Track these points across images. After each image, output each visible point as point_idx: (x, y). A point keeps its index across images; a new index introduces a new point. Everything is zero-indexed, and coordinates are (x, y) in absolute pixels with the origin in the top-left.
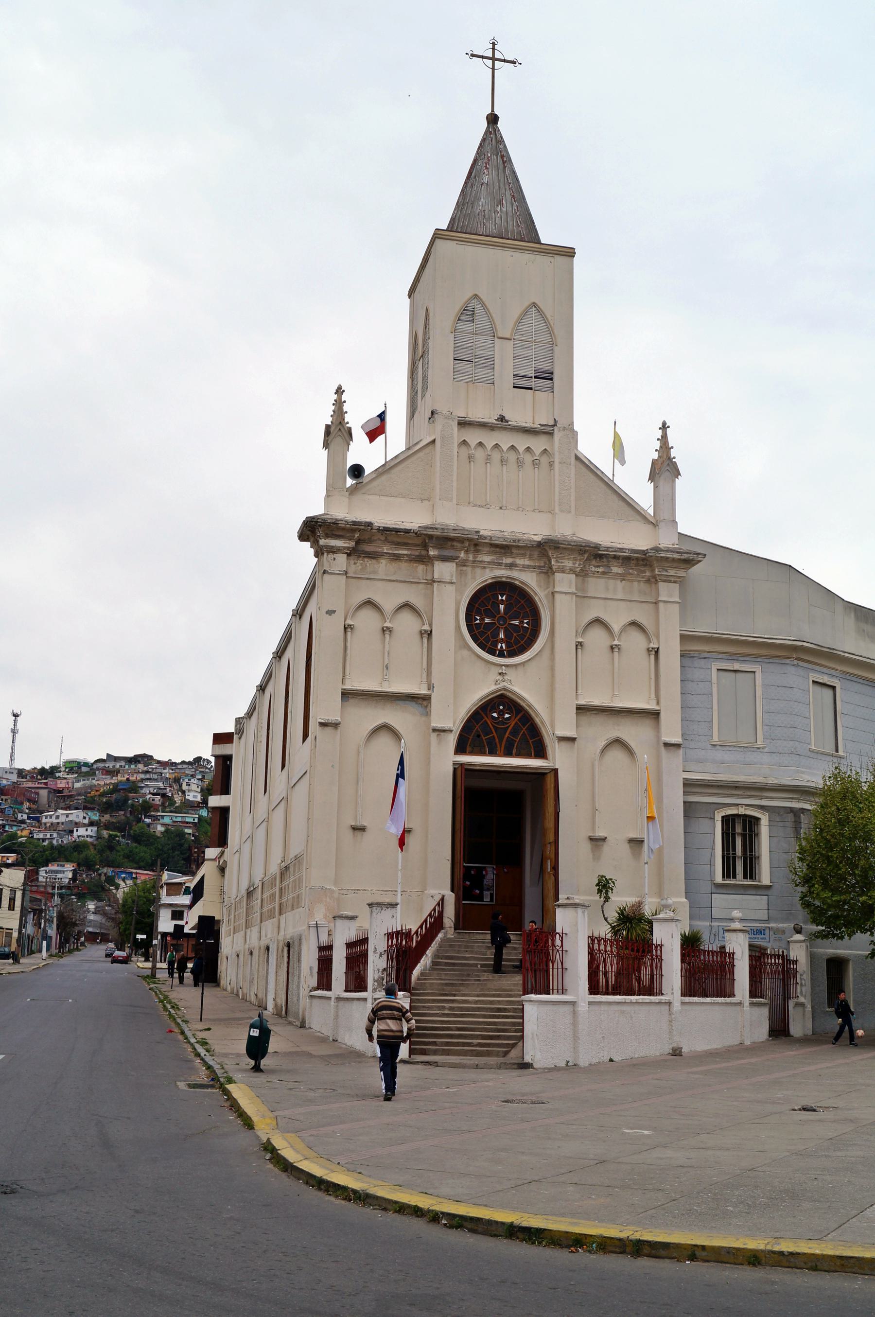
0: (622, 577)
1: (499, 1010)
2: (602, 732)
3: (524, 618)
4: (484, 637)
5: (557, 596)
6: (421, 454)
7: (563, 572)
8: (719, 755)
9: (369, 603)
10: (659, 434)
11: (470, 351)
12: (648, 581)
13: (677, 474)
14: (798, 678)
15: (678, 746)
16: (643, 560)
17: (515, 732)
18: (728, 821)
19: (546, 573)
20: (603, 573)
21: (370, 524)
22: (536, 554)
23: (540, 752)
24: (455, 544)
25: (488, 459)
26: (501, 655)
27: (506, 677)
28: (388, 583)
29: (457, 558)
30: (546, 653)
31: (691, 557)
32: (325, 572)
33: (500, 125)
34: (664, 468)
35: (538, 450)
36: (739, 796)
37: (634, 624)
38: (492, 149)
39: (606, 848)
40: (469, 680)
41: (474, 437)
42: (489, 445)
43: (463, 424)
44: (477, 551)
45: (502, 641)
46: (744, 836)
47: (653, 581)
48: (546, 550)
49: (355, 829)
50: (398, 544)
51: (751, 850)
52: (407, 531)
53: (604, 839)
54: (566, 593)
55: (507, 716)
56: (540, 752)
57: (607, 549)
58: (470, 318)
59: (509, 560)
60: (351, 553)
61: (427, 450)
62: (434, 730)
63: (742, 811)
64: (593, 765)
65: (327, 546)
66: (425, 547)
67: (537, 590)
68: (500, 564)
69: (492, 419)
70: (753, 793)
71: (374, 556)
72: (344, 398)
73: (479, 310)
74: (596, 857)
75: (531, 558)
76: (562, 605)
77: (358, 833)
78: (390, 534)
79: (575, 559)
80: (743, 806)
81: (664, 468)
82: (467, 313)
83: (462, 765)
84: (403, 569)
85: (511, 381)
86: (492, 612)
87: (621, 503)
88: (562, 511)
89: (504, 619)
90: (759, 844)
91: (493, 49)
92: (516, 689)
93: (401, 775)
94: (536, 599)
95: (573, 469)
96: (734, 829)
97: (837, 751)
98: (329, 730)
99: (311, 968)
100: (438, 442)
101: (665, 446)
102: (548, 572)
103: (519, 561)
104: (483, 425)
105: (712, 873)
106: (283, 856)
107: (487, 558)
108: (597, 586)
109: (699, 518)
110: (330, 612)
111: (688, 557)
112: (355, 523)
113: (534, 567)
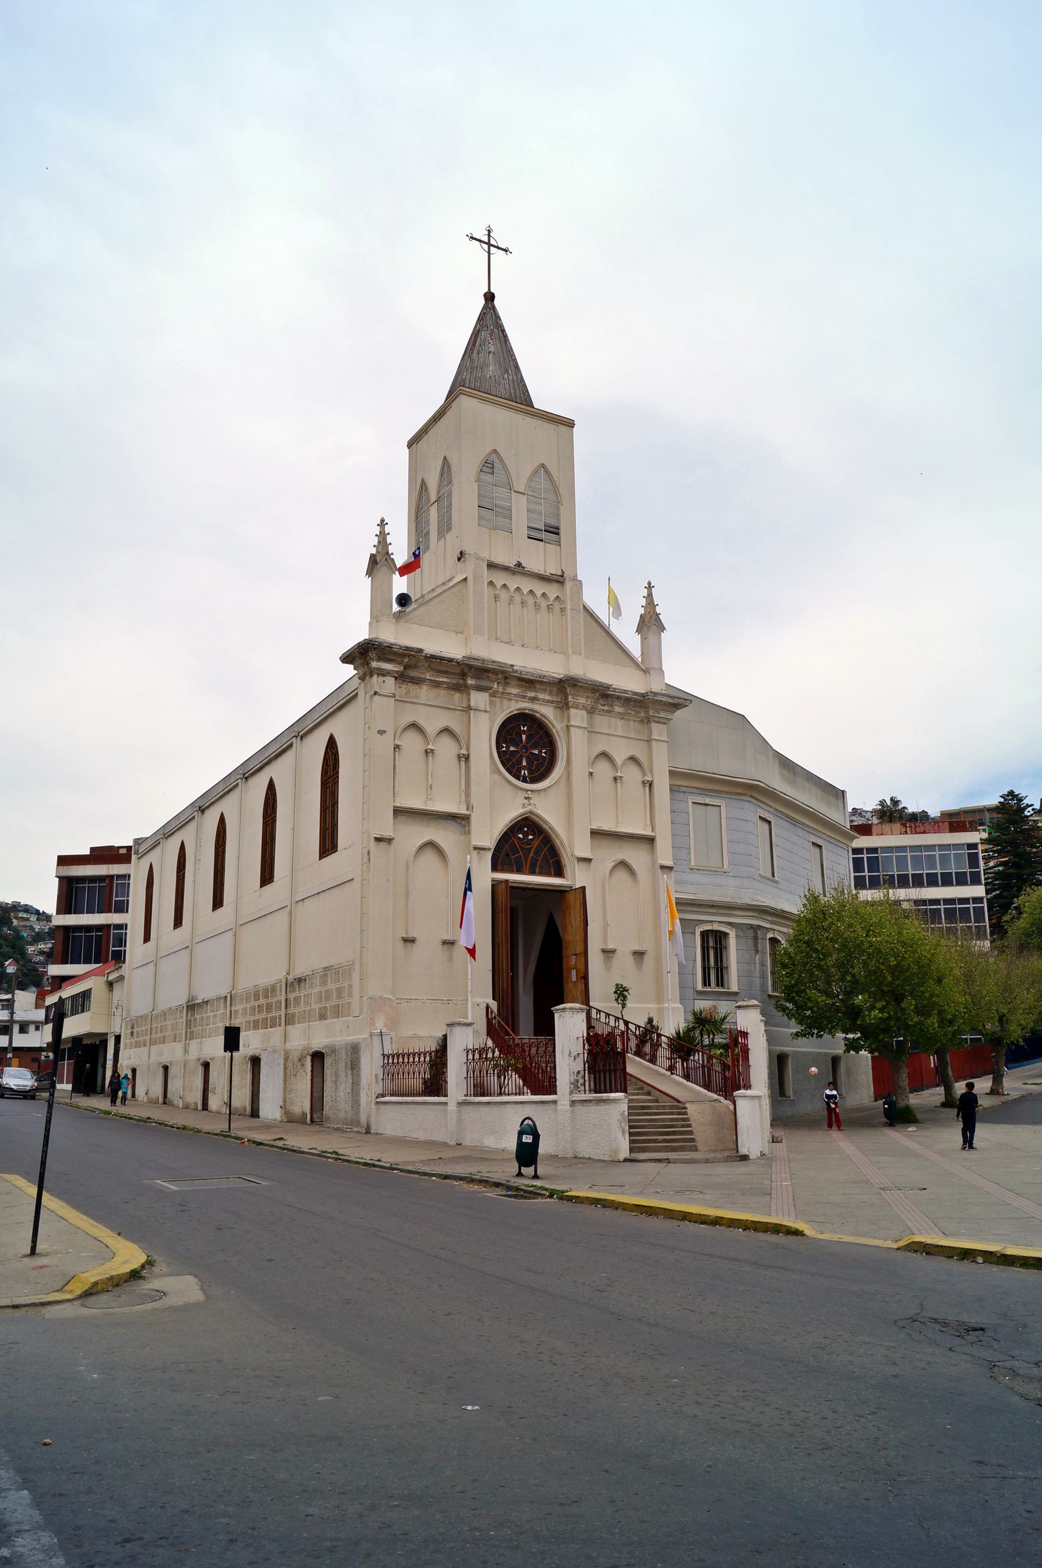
0: (622, 716)
1: (643, 1108)
2: (609, 855)
3: (544, 747)
4: (510, 762)
5: (572, 729)
6: (454, 590)
8: (696, 877)
9: (414, 726)
10: (645, 592)
12: (642, 721)
13: (663, 628)
14: (750, 811)
15: (670, 868)
16: (640, 701)
17: (537, 852)
18: (705, 935)
19: (561, 708)
20: (609, 712)
21: (420, 651)
22: (555, 690)
23: (559, 871)
24: (490, 675)
25: (511, 600)
26: (524, 780)
27: (532, 802)
28: (431, 708)
29: (490, 688)
30: (563, 781)
31: (681, 701)
32: (376, 693)
33: (496, 302)
34: (650, 623)
35: (552, 596)
36: (715, 914)
37: (632, 759)
38: (489, 321)
39: (616, 959)
41: (500, 579)
42: (512, 587)
43: (491, 566)
44: (507, 684)
45: (525, 768)
46: (715, 949)
47: (647, 721)
48: (564, 688)
49: (406, 940)
50: (440, 672)
51: (721, 961)
52: (450, 660)
53: (613, 951)
54: (580, 727)
55: (530, 837)
56: (559, 871)
58: (490, 470)
59: (531, 694)
60: (401, 677)
61: (459, 587)
62: (475, 848)
64: (603, 884)
65: (378, 669)
66: (463, 675)
67: (555, 723)
68: (524, 697)
69: (512, 564)
70: (725, 911)
71: (417, 681)
72: (387, 529)
73: (496, 461)
74: (608, 968)
75: (550, 694)
76: (576, 736)
77: (409, 945)
78: (436, 661)
79: (588, 697)
80: (716, 922)
81: (650, 623)
82: (489, 465)
83: (500, 882)
84: (441, 696)
85: (525, 532)
86: (516, 742)
88: (574, 653)
89: (527, 748)
90: (727, 957)
91: (489, 235)
92: (540, 812)
93: (468, 888)
94: (554, 731)
95: (582, 614)
97: (773, 876)
98: (383, 845)
99: (376, 1075)
100: (470, 581)
101: (650, 602)
102: (564, 706)
103: (541, 696)
104: (506, 569)
105: (694, 982)
106: (287, 968)
107: (514, 691)
108: (602, 722)
109: (682, 671)
110: (381, 732)
111: (677, 702)
112: (408, 649)
113: (552, 702)
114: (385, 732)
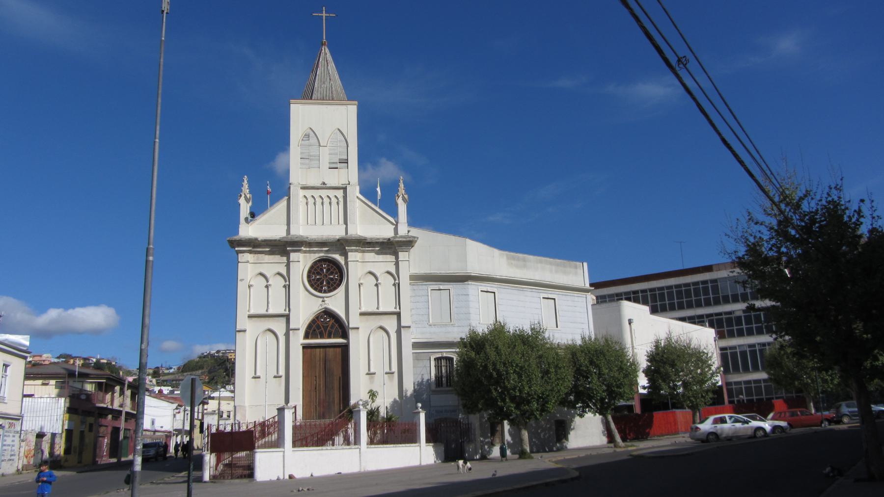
17: (332, 327)
26: (325, 292)
40: (306, 306)
41: (309, 193)
52: (275, 240)
57: (371, 239)
63: (445, 355)
69: (318, 184)
74: (372, 381)
76: (358, 265)
82: (307, 136)
85: (328, 166)
87: (727, 101)
89: (327, 275)
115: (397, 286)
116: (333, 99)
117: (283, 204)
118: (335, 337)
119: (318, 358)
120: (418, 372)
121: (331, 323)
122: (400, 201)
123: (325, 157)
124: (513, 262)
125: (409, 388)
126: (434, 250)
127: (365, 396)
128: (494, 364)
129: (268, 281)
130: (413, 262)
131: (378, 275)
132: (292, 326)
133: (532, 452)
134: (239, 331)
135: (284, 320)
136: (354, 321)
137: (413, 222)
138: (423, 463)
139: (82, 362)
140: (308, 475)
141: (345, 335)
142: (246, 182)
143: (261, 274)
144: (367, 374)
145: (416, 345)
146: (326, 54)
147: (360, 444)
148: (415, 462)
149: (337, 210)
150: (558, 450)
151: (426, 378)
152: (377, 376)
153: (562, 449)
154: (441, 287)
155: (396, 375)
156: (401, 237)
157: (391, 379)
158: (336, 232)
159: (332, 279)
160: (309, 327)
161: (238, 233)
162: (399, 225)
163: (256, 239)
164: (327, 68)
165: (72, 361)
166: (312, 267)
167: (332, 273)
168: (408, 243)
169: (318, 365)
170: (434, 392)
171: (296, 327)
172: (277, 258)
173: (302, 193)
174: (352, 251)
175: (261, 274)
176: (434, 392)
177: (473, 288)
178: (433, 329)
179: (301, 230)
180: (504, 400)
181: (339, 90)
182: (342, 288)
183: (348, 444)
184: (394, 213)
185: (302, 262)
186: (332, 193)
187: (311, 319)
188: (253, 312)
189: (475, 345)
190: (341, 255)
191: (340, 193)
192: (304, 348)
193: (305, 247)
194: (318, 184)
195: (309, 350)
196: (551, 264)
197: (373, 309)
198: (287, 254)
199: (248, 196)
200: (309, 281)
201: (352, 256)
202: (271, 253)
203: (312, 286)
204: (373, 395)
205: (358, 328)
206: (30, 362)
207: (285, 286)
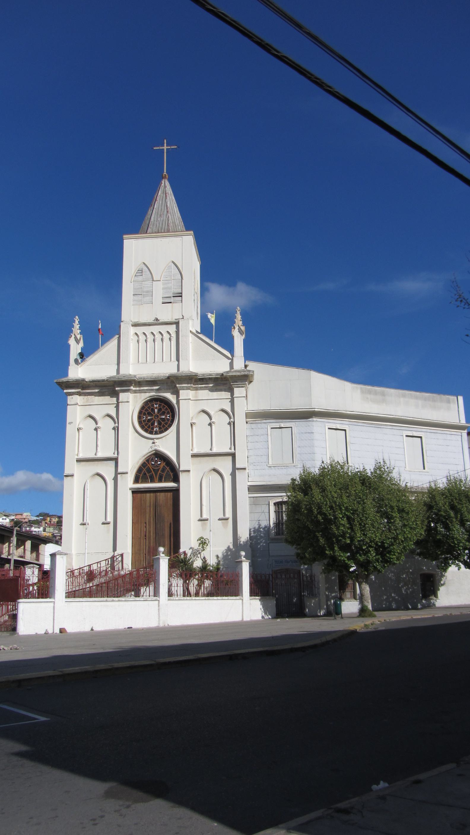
7: (184, 390)
11: (141, 290)
17: (163, 471)
26: (156, 433)
40: (135, 448)
41: (140, 330)
52: (103, 381)
57: (203, 375)
58: (141, 274)
76: (190, 404)
82: (140, 272)
85: (161, 301)
96: (282, 509)
114: (72, 423)
115: (232, 424)
116: (168, 231)
117: (114, 342)
118: (166, 481)
119: (148, 504)
120: (257, 516)
121: (162, 466)
122: (235, 333)
123: (159, 292)
124: (369, 396)
125: (244, 535)
126: (275, 384)
127: (195, 545)
128: (320, 508)
129: (97, 423)
130: (249, 399)
131: (212, 413)
132: (120, 470)
133: (375, 609)
134: (66, 476)
135: (113, 463)
136: (185, 463)
137: (249, 355)
138: (247, 618)
139: (57, 519)
140: (87, 629)
141: (176, 479)
142: (77, 322)
143: (91, 417)
144: (200, 520)
145: (252, 489)
146: (165, 187)
147: (159, 596)
148: (237, 618)
149: (169, 347)
150: (424, 607)
151: (264, 524)
152: (210, 525)
153: (430, 606)
154: (282, 425)
155: (230, 521)
156: (236, 371)
157: (225, 526)
158: (166, 368)
159: (163, 420)
160: (140, 470)
161: (67, 375)
162: (235, 359)
163: (83, 380)
164: (166, 202)
165: (48, 519)
166: (143, 408)
167: (163, 413)
168: (245, 378)
169: (148, 510)
170: (273, 540)
171: (124, 471)
172: (107, 399)
173: (133, 330)
174: (183, 389)
175: (91, 417)
176: (273, 540)
177: (319, 425)
178: (273, 471)
179: (132, 369)
180: (332, 549)
181: (177, 222)
182: (174, 428)
183: (189, 595)
184: (230, 348)
185: (132, 402)
186: (163, 329)
187: (141, 462)
188: (81, 456)
189: (306, 485)
190: (173, 393)
191: (172, 329)
192: (133, 492)
193: (135, 386)
194: (151, 320)
195: (139, 495)
196: (416, 398)
197: (206, 450)
198: (115, 394)
199: (78, 336)
200: (140, 422)
201: (183, 394)
202: (101, 394)
203: (142, 427)
204: (203, 542)
205: (189, 471)
206: (13, 520)
207: (114, 429)
